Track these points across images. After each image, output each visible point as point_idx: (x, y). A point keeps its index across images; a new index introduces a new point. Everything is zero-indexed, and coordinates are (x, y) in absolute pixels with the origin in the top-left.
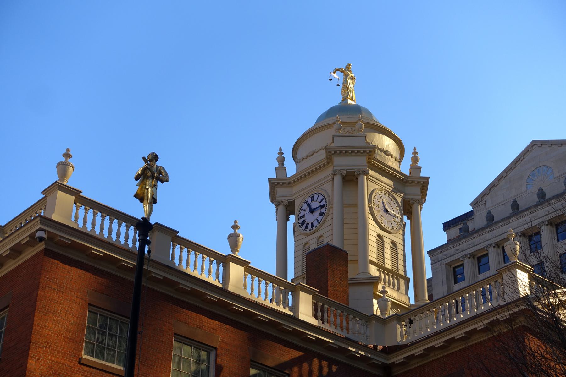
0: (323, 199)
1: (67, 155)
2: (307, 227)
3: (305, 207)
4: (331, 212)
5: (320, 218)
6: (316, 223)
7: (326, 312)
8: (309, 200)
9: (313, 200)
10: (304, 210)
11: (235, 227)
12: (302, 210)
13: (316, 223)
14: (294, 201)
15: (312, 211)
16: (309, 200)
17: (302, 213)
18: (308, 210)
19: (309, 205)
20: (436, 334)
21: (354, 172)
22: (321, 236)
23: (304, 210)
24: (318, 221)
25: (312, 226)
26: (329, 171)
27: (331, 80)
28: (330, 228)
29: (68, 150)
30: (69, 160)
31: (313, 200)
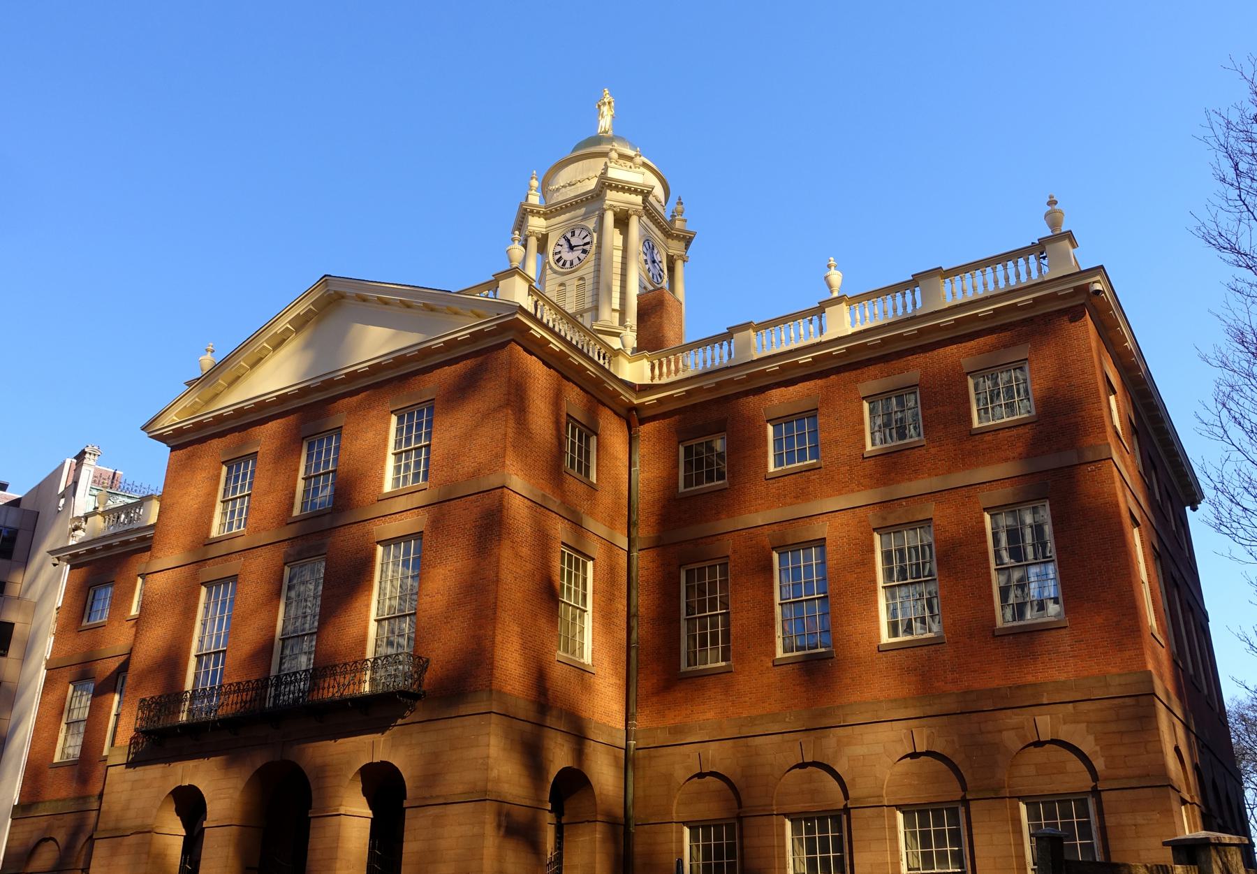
1: (1052, 202)
2: (564, 264)
3: (563, 241)
5: (582, 256)
6: (576, 262)
8: (569, 235)
9: (573, 235)
11: (1052, 202)
13: (576, 262)
15: (571, 248)
16: (569, 235)
18: (566, 246)
19: (568, 241)
20: (545, 327)
25: (572, 263)
29: (1051, 197)
30: (1056, 207)
31: (573, 235)
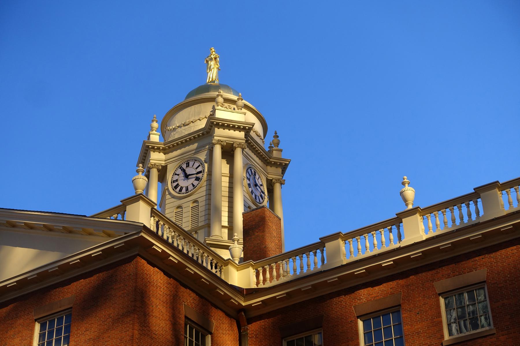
2: (181, 190)
10: (178, 175)
12: (176, 174)
17: (176, 177)
23: (178, 175)
24: (193, 185)
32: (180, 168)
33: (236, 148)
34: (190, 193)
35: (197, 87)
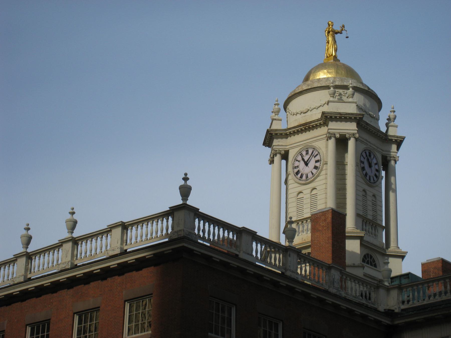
0: (317, 155)
2: (301, 177)
3: (299, 158)
4: (324, 168)
5: (315, 171)
6: (310, 175)
7: (343, 282)
10: (299, 161)
12: (297, 160)
13: (310, 175)
14: (288, 150)
16: (304, 153)
17: (297, 164)
21: (346, 135)
22: (301, 192)
23: (299, 161)
24: (312, 173)
25: (307, 177)
26: (323, 130)
27: (347, 37)
28: (324, 181)
32: (301, 155)
33: (336, 75)
34: (321, 167)
35: (360, 76)
